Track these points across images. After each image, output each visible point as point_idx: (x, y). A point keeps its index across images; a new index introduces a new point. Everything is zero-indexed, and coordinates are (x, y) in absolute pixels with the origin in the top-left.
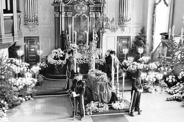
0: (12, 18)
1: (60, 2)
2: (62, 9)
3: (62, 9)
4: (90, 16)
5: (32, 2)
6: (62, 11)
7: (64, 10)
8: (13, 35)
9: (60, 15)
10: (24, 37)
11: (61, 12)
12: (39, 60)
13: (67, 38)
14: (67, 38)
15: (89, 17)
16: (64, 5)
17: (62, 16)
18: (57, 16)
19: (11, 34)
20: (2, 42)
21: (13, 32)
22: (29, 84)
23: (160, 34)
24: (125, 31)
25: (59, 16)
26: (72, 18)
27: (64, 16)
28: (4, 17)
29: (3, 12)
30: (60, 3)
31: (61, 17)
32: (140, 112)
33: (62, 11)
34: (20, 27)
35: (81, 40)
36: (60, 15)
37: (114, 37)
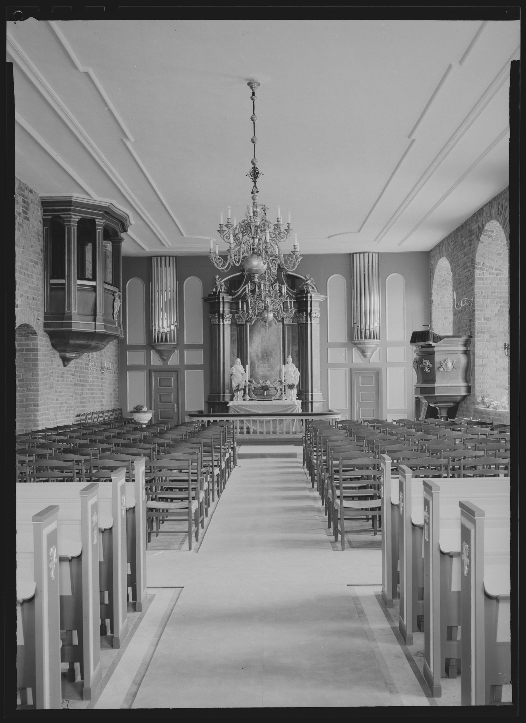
0: (94, 288)
1: (219, 291)
2: (224, 308)
3: (224, 308)
4: (285, 322)
7: (229, 310)
8: (95, 320)
9: (221, 320)
10: (418, 616)
11: (223, 314)
16: (227, 298)
17: (226, 322)
19: (92, 318)
20: (71, 327)
21: (95, 315)
23: (451, 64)
25: (219, 321)
26: (246, 325)
27: (230, 323)
28: (78, 285)
29: (76, 278)
30: (219, 295)
32: (296, 383)
34: (113, 313)
35: (267, 374)
36: (221, 320)
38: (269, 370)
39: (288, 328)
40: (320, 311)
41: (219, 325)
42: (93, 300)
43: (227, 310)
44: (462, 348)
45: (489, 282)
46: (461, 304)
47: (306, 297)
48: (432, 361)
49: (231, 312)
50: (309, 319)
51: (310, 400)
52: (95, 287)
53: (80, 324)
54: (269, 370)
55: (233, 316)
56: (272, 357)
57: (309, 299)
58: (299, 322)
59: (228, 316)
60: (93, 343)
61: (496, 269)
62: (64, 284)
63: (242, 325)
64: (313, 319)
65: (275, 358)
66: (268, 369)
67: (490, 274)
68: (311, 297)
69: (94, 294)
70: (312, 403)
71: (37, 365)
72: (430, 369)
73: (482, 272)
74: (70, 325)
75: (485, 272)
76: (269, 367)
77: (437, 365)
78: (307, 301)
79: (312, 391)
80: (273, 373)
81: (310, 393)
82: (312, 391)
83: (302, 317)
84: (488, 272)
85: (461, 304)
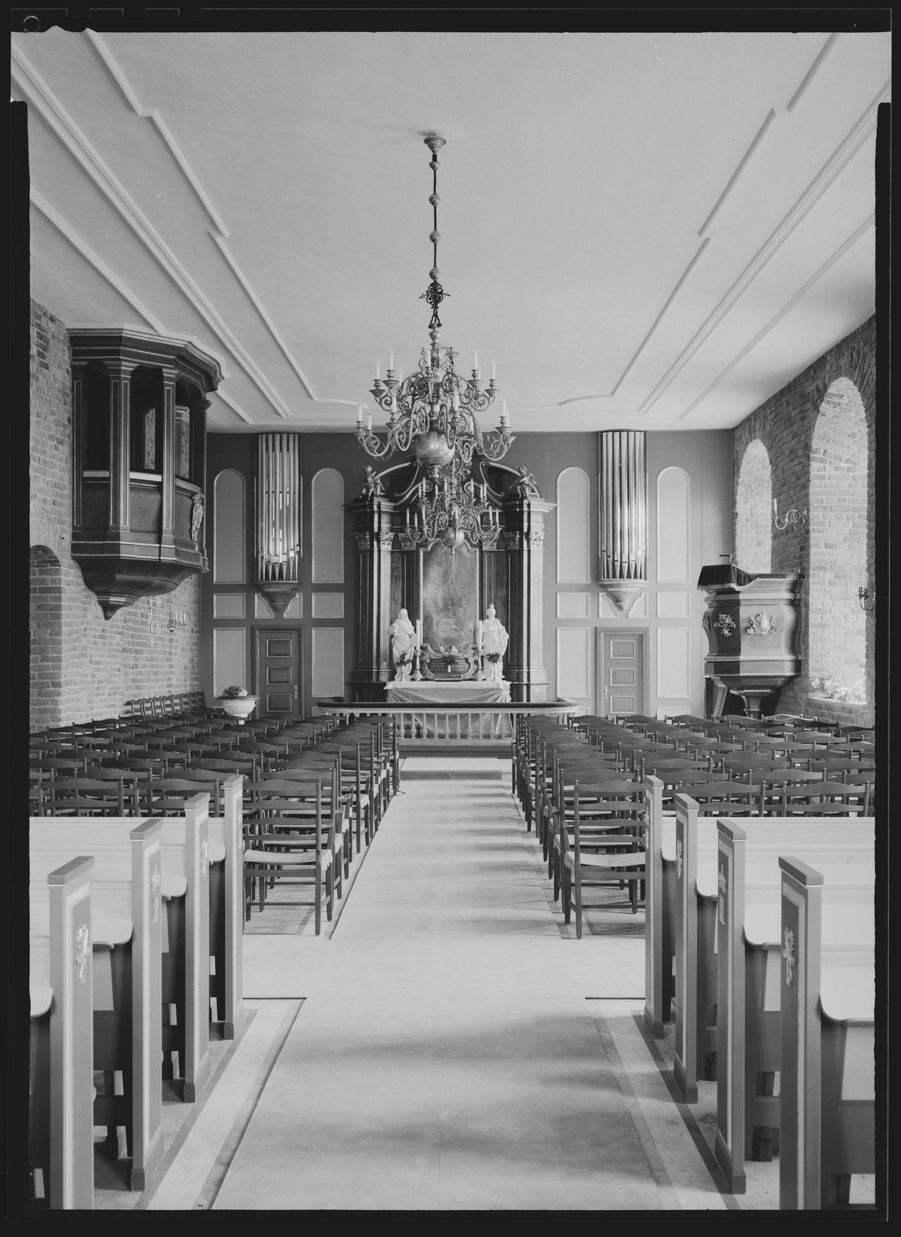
0: (159, 487)
1: (373, 493)
4: (485, 548)
5: (276, 476)
6: (379, 528)
9: (375, 543)
11: (378, 534)
12: (373, 505)
13: (495, 635)
14: (495, 635)
15: (478, 550)
16: (386, 506)
18: (283, 849)
22: (389, 421)
24: (110, 622)
25: (372, 546)
26: (417, 552)
27: (389, 548)
28: (132, 480)
30: (372, 500)
31: (376, 548)
33: (379, 528)
34: (191, 529)
36: (375, 543)
37: (634, 641)
38: (456, 630)
39: (489, 557)
40: (545, 530)
41: (372, 551)
42: (156, 505)
43: (385, 526)
44: (788, 596)
45: (835, 482)
46: (787, 520)
47: (521, 506)
48: (736, 617)
49: (392, 530)
50: (525, 542)
51: (525, 681)
52: (160, 485)
53: (134, 547)
54: (456, 630)
55: (396, 537)
56: (461, 606)
57: (525, 509)
58: (509, 548)
59: (387, 537)
60: (156, 580)
61: (848, 461)
62: (108, 479)
63: (412, 552)
64: (531, 542)
65: (466, 609)
66: (455, 627)
67: (836, 469)
68: (529, 506)
69: (159, 497)
70: (528, 686)
71: (59, 617)
72: (731, 630)
73: (822, 465)
74: (116, 548)
75: (827, 465)
76: (456, 624)
77: (743, 625)
78: (522, 512)
79: (528, 665)
80: (463, 634)
81: (525, 670)
82: (528, 665)
83: (514, 539)
84: (834, 466)
85: (787, 520)
